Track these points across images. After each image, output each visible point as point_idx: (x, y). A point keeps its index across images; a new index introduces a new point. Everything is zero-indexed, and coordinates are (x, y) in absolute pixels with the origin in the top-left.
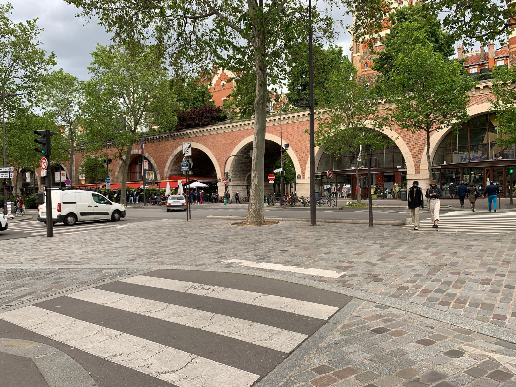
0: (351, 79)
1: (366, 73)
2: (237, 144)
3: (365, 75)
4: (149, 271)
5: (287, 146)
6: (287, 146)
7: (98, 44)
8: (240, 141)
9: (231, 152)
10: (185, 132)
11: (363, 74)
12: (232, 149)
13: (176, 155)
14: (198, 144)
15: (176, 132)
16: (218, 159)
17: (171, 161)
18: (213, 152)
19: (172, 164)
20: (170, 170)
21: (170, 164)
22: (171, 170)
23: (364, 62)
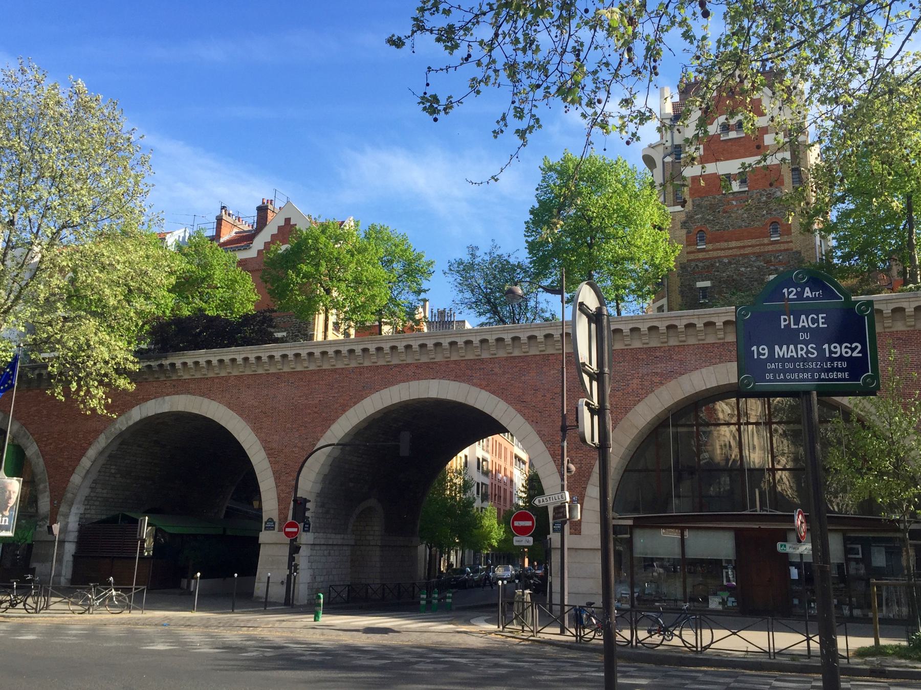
0: (901, 227)
1: (701, 256)
2: (344, 408)
3: (698, 260)
4: (280, 652)
5: (225, 530)
6: (225, 530)
7: (436, 120)
8: (357, 398)
9: (323, 432)
10: (166, 362)
11: (692, 257)
12: (328, 422)
13: (121, 434)
14: (206, 401)
15: (157, 359)
16: (271, 453)
17: (101, 453)
18: (257, 430)
19: (102, 461)
20: (88, 482)
21: (94, 462)
22: (95, 482)
23: (694, 227)
